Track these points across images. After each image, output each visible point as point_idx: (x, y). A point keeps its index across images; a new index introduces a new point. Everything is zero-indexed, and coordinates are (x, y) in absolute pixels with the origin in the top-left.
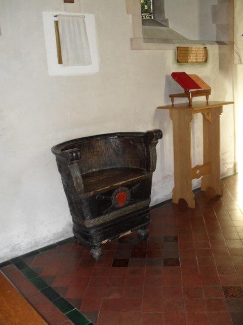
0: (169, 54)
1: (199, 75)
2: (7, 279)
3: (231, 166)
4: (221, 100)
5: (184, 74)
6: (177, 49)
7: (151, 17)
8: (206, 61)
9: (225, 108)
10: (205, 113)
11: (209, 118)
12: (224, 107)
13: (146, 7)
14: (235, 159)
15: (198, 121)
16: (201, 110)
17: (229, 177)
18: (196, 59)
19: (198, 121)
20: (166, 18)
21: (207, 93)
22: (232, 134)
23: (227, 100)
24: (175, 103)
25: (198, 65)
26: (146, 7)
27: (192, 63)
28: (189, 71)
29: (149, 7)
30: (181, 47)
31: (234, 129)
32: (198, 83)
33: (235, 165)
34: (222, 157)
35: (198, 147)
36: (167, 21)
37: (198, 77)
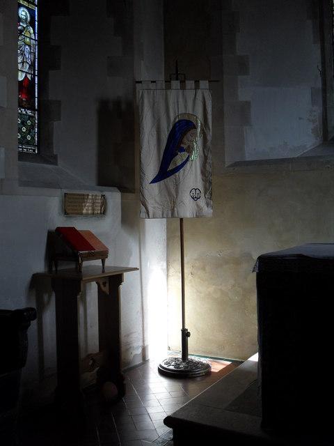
0: (54, 203)
1: (94, 231)
2: (36, 65)
3: (139, 351)
4: (123, 265)
5: (73, 229)
6: (65, 196)
7: (34, 151)
8: (104, 213)
9: (127, 276)
10: (101, 283)
11: (106, 289)
12: (126, 275)
13: (29, 138)
14: (143, 341)
15: (92, 294)
16: (96, 278)
17: (137, 366)
18: (93, 210)
19: (92, 294)
20: (55, 153)
21: (103, 255)
22: (139, 309)
23: (131, 266)
24: (58, 269)
25: (94, 218)
26: (29, 138)
27: (87, 215)
28: (80, 225)
29: (33, 138)
30: (70, 194)
31: (142, 302)
32: (91, 242)
33: (144, 349)
34: (253, 300)
35: (91, 327)
36: (55, 157)
37: (93, 235)
